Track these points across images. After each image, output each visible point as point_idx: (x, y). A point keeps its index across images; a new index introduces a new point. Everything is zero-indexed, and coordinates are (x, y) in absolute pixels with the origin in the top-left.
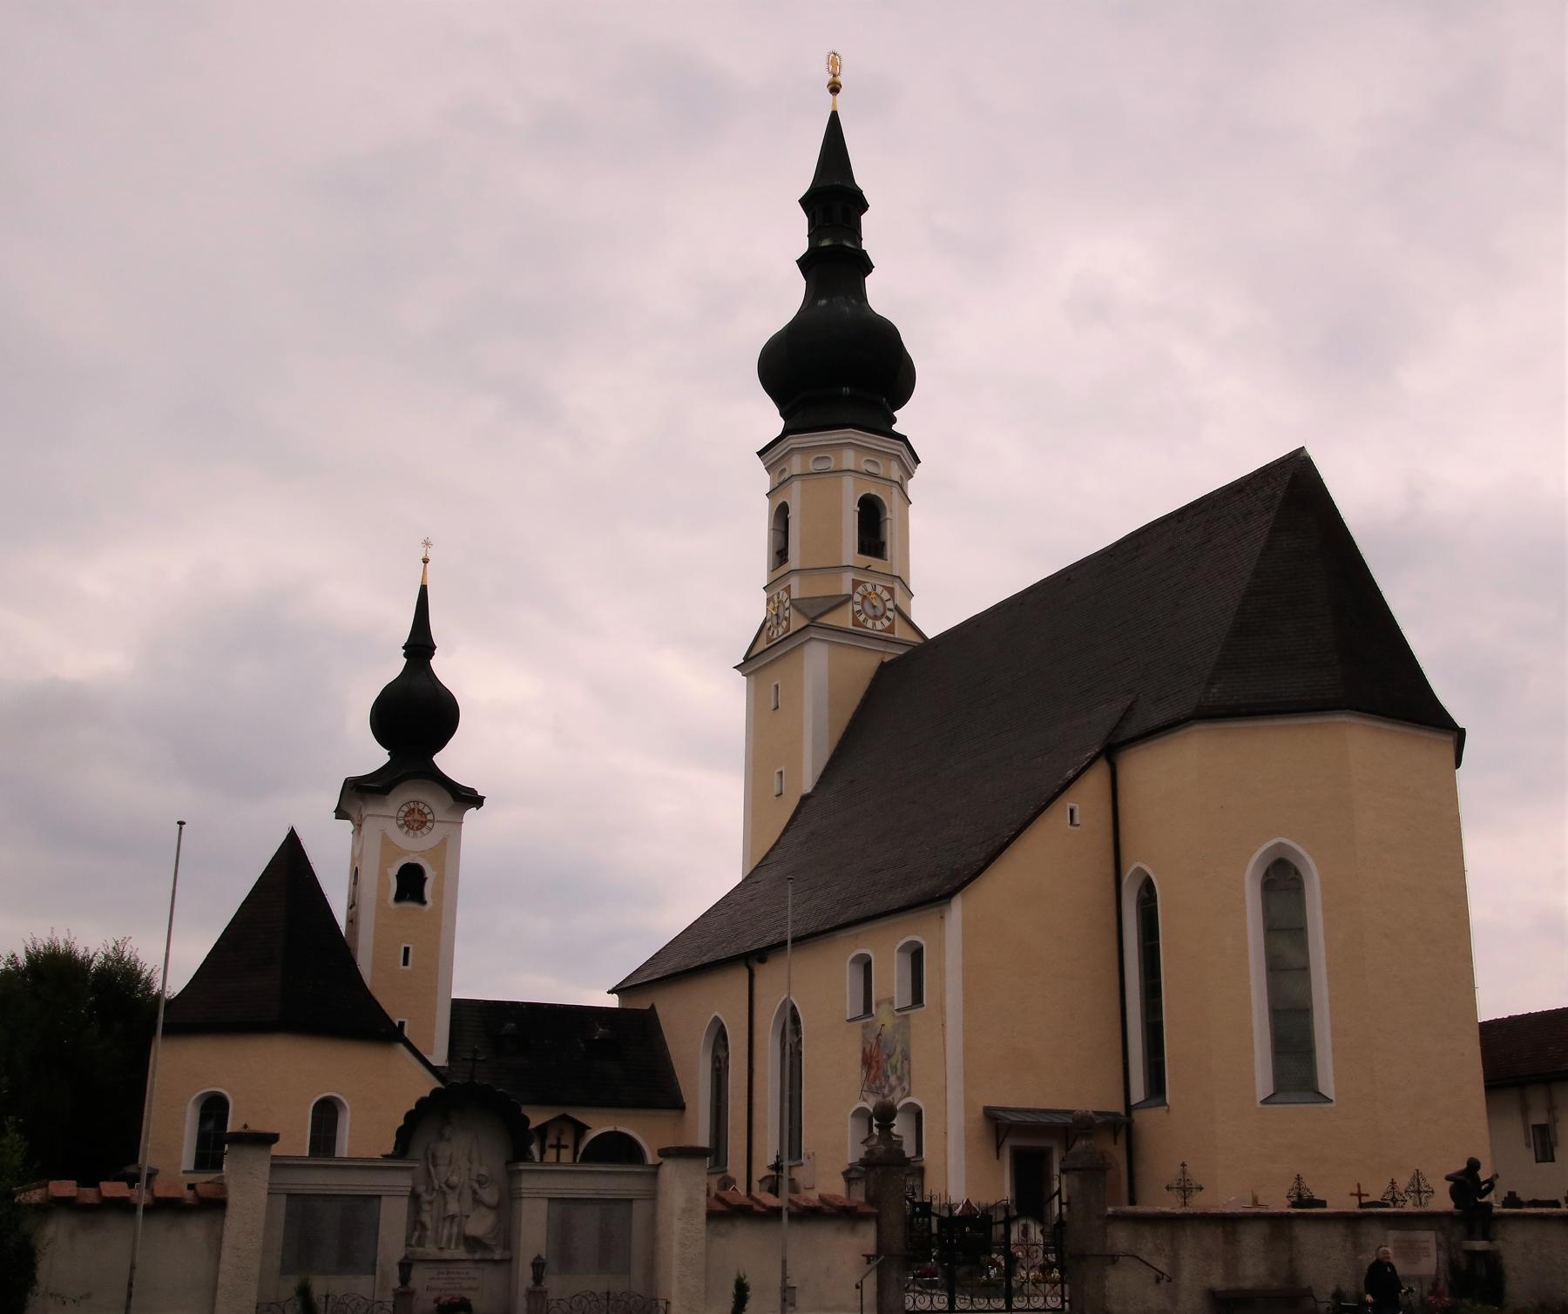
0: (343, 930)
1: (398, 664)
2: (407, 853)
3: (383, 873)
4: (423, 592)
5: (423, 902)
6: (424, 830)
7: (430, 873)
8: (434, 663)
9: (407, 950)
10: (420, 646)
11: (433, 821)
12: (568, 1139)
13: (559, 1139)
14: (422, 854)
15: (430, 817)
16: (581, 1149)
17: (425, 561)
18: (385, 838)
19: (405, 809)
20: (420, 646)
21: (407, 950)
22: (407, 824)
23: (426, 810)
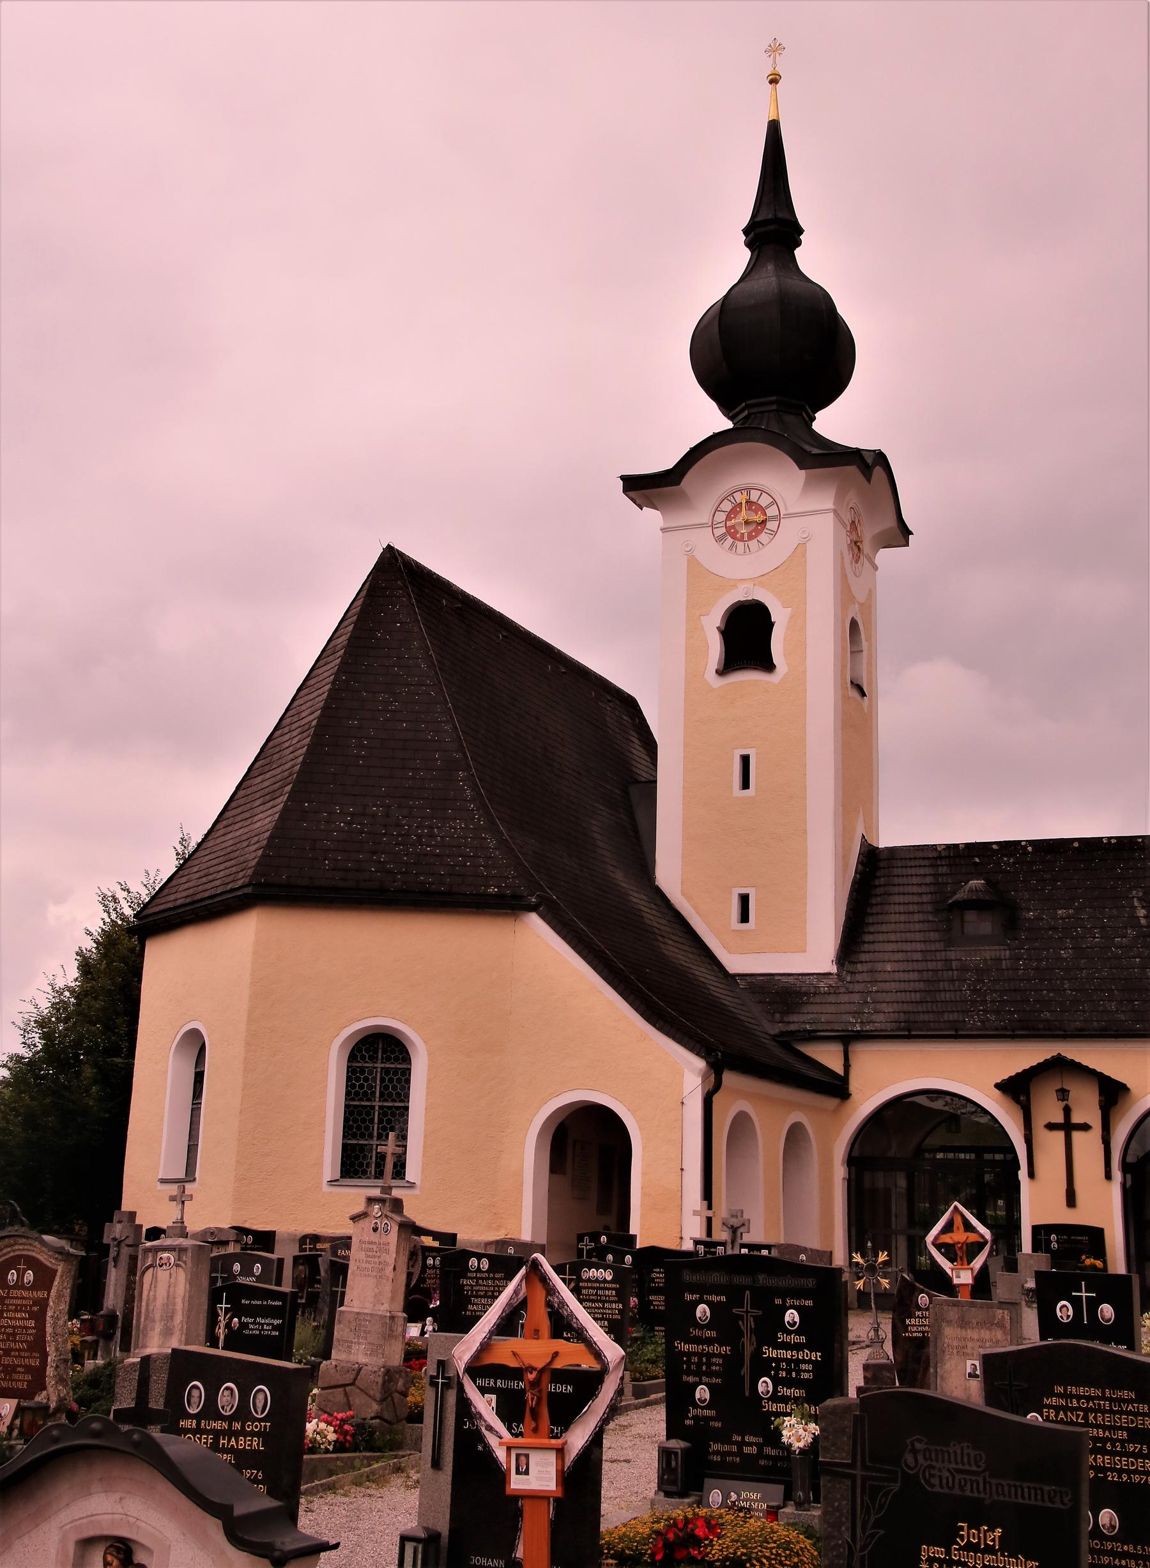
1: (735, 259)
2: (734, 584)
4: (774, 130)
5: (767, 664)
6: (763, 537)
7: (778, 614)
8: (798, 252)
9: (745, 760)
10: (773, 229)
11: (778, 518)
12: (1087, 1110)
13: (1067, 1111)
14: (760, 580)
15: (772, 512)
16: (129, 1450)
17: (774, 81)
18: (693, 564)
19: (727, 506)
20: (773, 229)
22: (732, 532)
23: (764, 501)
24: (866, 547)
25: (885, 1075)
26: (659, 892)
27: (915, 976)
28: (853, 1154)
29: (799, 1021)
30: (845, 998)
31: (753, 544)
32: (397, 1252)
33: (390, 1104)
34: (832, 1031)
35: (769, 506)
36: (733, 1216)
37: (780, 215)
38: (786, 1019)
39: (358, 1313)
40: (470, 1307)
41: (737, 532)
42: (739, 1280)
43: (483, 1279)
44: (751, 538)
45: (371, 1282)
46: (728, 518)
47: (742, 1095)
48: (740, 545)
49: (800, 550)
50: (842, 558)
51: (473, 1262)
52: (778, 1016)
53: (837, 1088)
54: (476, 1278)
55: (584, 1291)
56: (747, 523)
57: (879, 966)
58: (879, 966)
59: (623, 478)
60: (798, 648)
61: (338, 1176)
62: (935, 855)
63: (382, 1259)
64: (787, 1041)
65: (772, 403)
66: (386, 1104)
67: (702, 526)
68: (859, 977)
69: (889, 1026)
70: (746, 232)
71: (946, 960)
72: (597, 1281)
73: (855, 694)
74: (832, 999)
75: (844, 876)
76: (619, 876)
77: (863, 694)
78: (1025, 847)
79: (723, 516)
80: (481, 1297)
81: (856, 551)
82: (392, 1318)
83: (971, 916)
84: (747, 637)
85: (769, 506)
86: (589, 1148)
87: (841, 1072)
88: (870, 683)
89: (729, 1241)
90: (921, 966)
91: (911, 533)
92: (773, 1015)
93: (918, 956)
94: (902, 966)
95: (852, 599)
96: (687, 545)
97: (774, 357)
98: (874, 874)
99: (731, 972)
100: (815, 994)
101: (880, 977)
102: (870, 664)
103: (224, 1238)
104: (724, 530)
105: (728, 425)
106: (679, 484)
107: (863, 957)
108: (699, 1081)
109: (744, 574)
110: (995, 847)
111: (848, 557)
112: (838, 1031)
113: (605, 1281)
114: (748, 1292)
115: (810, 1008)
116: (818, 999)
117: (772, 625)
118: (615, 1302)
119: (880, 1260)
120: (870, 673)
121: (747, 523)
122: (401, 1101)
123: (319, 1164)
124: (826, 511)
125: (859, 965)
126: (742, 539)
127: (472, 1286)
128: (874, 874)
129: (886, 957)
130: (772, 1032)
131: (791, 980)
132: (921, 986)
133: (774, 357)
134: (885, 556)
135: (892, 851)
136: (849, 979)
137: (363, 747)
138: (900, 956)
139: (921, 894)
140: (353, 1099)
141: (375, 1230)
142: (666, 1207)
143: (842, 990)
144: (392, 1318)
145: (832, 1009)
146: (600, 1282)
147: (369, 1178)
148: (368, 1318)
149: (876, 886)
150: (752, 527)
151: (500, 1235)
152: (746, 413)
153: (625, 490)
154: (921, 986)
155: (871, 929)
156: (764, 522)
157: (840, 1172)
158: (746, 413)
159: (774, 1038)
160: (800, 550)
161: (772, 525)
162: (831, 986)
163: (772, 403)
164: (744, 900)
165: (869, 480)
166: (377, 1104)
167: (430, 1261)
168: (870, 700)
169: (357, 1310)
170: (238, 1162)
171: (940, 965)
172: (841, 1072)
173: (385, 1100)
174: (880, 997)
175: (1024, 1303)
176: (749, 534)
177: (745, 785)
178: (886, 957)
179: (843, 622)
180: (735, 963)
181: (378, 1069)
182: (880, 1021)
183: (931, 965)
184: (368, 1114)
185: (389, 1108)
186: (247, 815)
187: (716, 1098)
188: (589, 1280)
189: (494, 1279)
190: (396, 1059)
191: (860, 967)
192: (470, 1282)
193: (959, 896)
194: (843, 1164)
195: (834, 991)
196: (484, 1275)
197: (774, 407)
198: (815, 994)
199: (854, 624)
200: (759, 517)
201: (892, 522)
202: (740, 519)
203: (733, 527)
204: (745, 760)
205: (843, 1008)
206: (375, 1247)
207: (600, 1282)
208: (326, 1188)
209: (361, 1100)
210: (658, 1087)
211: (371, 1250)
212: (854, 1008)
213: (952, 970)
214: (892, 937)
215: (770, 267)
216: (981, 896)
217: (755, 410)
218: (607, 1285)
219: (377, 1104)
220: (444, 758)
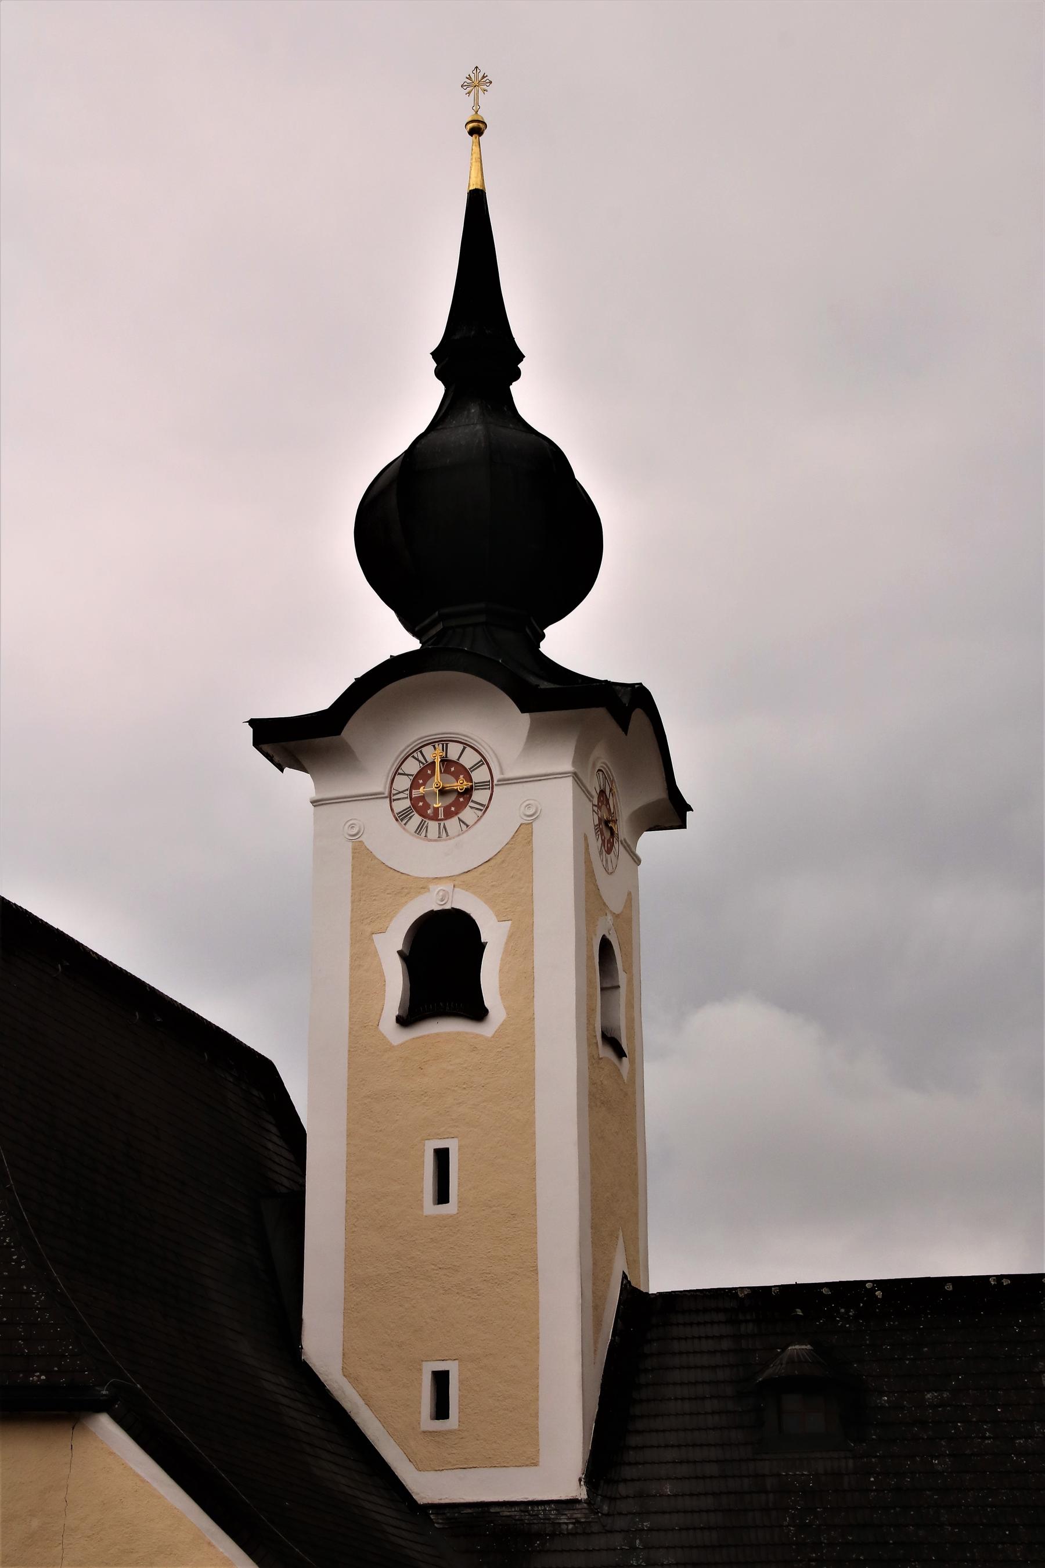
0: (625, 1078)
1: (418, 401)
2: (422, 885)
3: (362, 953)
5: (478, 1012)
7: (492, 932)
9: (442, 1157)
10: (478, 349)
11: (489, 785)
14: (464, 879)
15: (480, 775)
17: (477, 130)
19: (412, 767)
20: (478, 349)
21: (442, 1157)
22: (420, 806)
23: (469, 759)
24: (623, 829)
31: (452, 824)
41: (427, 806)
44: (449, 814)
46: (414, 785)
48: (433, 825)
56: (443, 792)
59: (253, 723)
67: (375, 796)
73: (607, 1053)
75: (596, 1342)
78: (872, 1291)
81: (607, 835)
84: (444, 966)
88: (631, 1037)
97: (479, 536)
100: (553, 1535)
104: (407, 803)
109: (438, 868)
111: (595, 844)
117: (483, 946)
121: (443, 792)
124: (562, 775)
126: (435, 817)
131: (514, 1512)
133: (479, 536)
150: (450, 799)
153: (257, 743)
156: (468, 792)
162: (577, 1522)
164: (441, 1379)
168: (632, 1062)
177: (442, 1196)
179: (589, 943)
180: (429, 1486)
197: (482, 619)
198: (553, 1535)
199: (606, 946)
200: (460, 784)
203: (422, 798)
215: (474, 410)
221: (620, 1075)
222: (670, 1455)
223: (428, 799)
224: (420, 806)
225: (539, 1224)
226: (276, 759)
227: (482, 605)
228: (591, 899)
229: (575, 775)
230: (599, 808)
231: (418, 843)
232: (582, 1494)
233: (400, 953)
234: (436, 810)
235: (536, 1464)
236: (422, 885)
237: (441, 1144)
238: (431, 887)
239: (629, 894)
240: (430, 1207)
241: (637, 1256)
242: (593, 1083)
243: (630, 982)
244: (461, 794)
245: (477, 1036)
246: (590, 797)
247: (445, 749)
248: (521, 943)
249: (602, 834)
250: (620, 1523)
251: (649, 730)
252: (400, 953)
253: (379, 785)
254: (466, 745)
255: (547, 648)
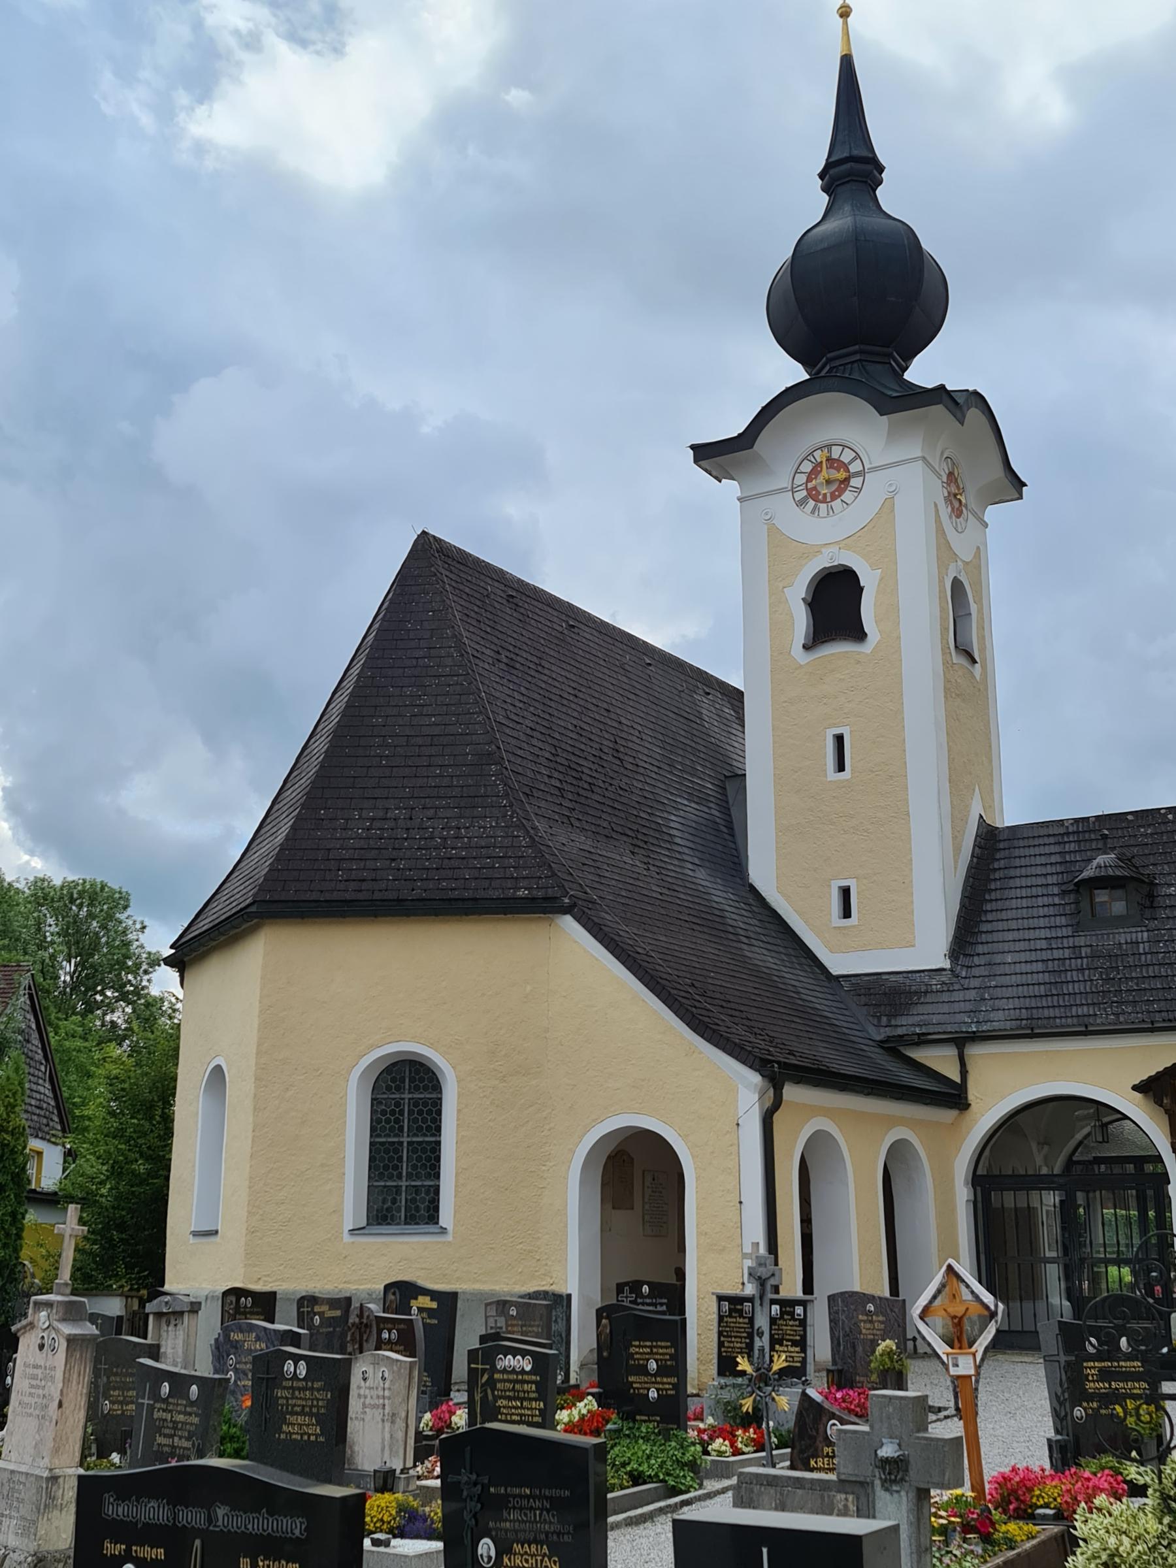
0: (978, 678)
1: (809, 205)
2: (817, 550)
4: (847, 67)
5: (859, 635)
6: (847, 496)
9: (839, 739)
10: (852, 168)
11: (861, 473)
14: (847, 543)
15: (855, 467)
18: (773, 531)
19: (807, 467)
20: (852, 168)
22: (813, 494)
23: (847, 456)
24: (969, 499)
25: (1008, 1080)
26: (753, 890)
27: (1040, 966)
28: (979, 1172)
29: (906, 1025)
30: (959, 996)
31: (837, 504)
32: (66, 1381)
33: (420, 1139)
34: (944, 1033)
35: (851, 462)
36: (760, 1265)
37: (855, 153)
38: (893, 1023)
39: (12, 1472)
40: (285, 1428)
41: (818, 493)
42: (192, 1517)
43: (299, 1389)
44: (834, 498)
45: (33, 1423)
46: (809, 480)
47: (812, 1111)
48: (823, 506)
49: (889, 505)
50: (937, 511)
51: (289, 1366)
52: (884, 1019)
53: (954, 1097)
54: (292, 1387)
55: (499, 1385)
56: (829, 482)
57: (998, 959)
58: (998, 959)
59: (693, 447)
60: (891, 612)
61: (364, 1223)
62: (1062, 830)
63: (46, 1392)
64: (893, 1047)
65: (855, 353)
66: (415, 1139)
67: (782, 490)
68: (976, 972)
69: (1008, 1025)
70: (822, 176)
71: (1074, 947)
72: (514, 1371)
73: (963, 661)
74: (945, 997)
75: (956, 862)
76: (702, 876)
77: (974, 661)
78: (1165, 815)
79: (803, 478)
80: (297, 1414)
81: (957, 505)
82: (54, 1479)
83: (1102, 896)
84: (835, 605)
85: (851, 462)
86: (639, 1178)
87: (958, 1080)
88: (983, 650)
89: (757, 1296)
90: (1046, 955)
91: (1024, 485)
92: (879, 1018)
93: (1043, 944)
94: (1023, 957)
95: (955, 557)
96: (766, 514)
97: (859, 308)
98: (993, 857)
99: (834, 973)
100: (926, 992)
101: (999, 970)
102: (981, 628)
103: (178, 1309)
104: (804, 493)
105: (808, 377)
106: (752, 447)
107: (980, 949)
108: (756, 1097)
109: (827, 537)
110: (1130, 817)
111: (945, 511)
112: (951, 1033)
113: (523, 1372)
114: (198, 1542)
115: (921, 1009)
116: (929, 998)
117: (862, 589)
118: (536, 1400)
119: (775, 1367)
120: (982, 639)
121: (829, 482)
122: (433, 1135)
123: (338, 1211)
124: (915, 459)
125: (976, 958)
126: (824, 501)
127: (287, 1398)
128: (993, 857)
129: (1006, 947)
130: (878, 1038)
131: (899, 978)
132: (1046, 977)
133: (859, 308)
134: (993, 513)
135: (1015, 831)
136: (964, 974)
137: (388, 746)
138: (1022, 945)
139: (1045, 875)
140: (379, 1136)
141: (41, 1347)
142: (720, 1249)
143: (956, 987)
144: (54, 1479)
145: (946, 1008)
146: (517, 1373)
147: (398, 1224)
148: (23, 1479)
149: (995, 870)
150: (834, 487)
151: (532, 1288)
152: (828, 368)
153: (696, 461)
154: (1046, 977)
155: (990, 917)
156: (846, 480)
157: (962, 1194)
158: (828, 368)
159: (881, 1044)
160: (889, 505)
161: (855, 482)
162: (944, 983)
163: (855, 353)
164: (846, 892)
165: (962, 424)
166: (405, 1140)
167: (385, 1335)
168: (984, 668)
169: (11, 1467)
170: (249, 1212)
171: (1067, 953)
172: (958, 1080)
173: (415, 1135)
174: (999, 992)
175: (877, 1482)
176: (832, 494)
177: (841, 767)
178: (1006, 947)
179: (941, 581)
180: (839, 964)
181: (406, 1103)
182: (999, 1021)
183: (1057, 954)
184: (396, 1151)
185: (419, 1143)
186: (275, 829)
187: (777, 1117)
188: (504, 1371)
189: (312, 1389)
190: (426, 1088)
191: (976, 960)
192: (286, 1393)
193: (1086, 874)
194: (966, 1183)
195: (948, 988)
196: (300, 1384)
197: (857, 357)
198: (926, 992)
199: (957, 585)
200: (842, 475)
201: (999, 472)
202: (821, 479)
203: (815, 488)
204: (839, 739)
205: (956, 1007)
206: (39, 1372)
207: (517, 1373)
208: (347, 1238)
209: (389, 1136)
210: (711, 1111)
211: (34, 1377)
212: (968, 1006)
213: (1081, 958)
214: (1013, 925)
215: (847, 208)
216: (1110, 872)
217: (837, 363)
218: (526, 1377)
219: (405, 1140)
220: (481, 753)
221: (973, 677)
222: (1010, 936)
223: (819, 488)
224: (813, 494)
225: (174, 1156)
226: (714, 473)
227: (857, 347)
228: (944, 551)
229: (924, 458)
230: (949, 485)
231: (814, 519)
232: (947, 964)
233: (803, 599)
234: (825, 495)
235: (913, 946)
236: (817, 550)
237: (838, 731)
238: (823, 550)
239: (978, 548)
240: (832, 775)
241: (990, 796)
242: (947, 681)
243: (980, 611)
244: (842, 482)
245: (859, 653)
246: (939, 476)
247: (830, 451)
248: (889, 583)
249: (951, 504)
250: (975, 983)
251: (984, 420)
252: (803, 599)
253: (785, 483)
254: (845, 446)
255: (907, 376)
